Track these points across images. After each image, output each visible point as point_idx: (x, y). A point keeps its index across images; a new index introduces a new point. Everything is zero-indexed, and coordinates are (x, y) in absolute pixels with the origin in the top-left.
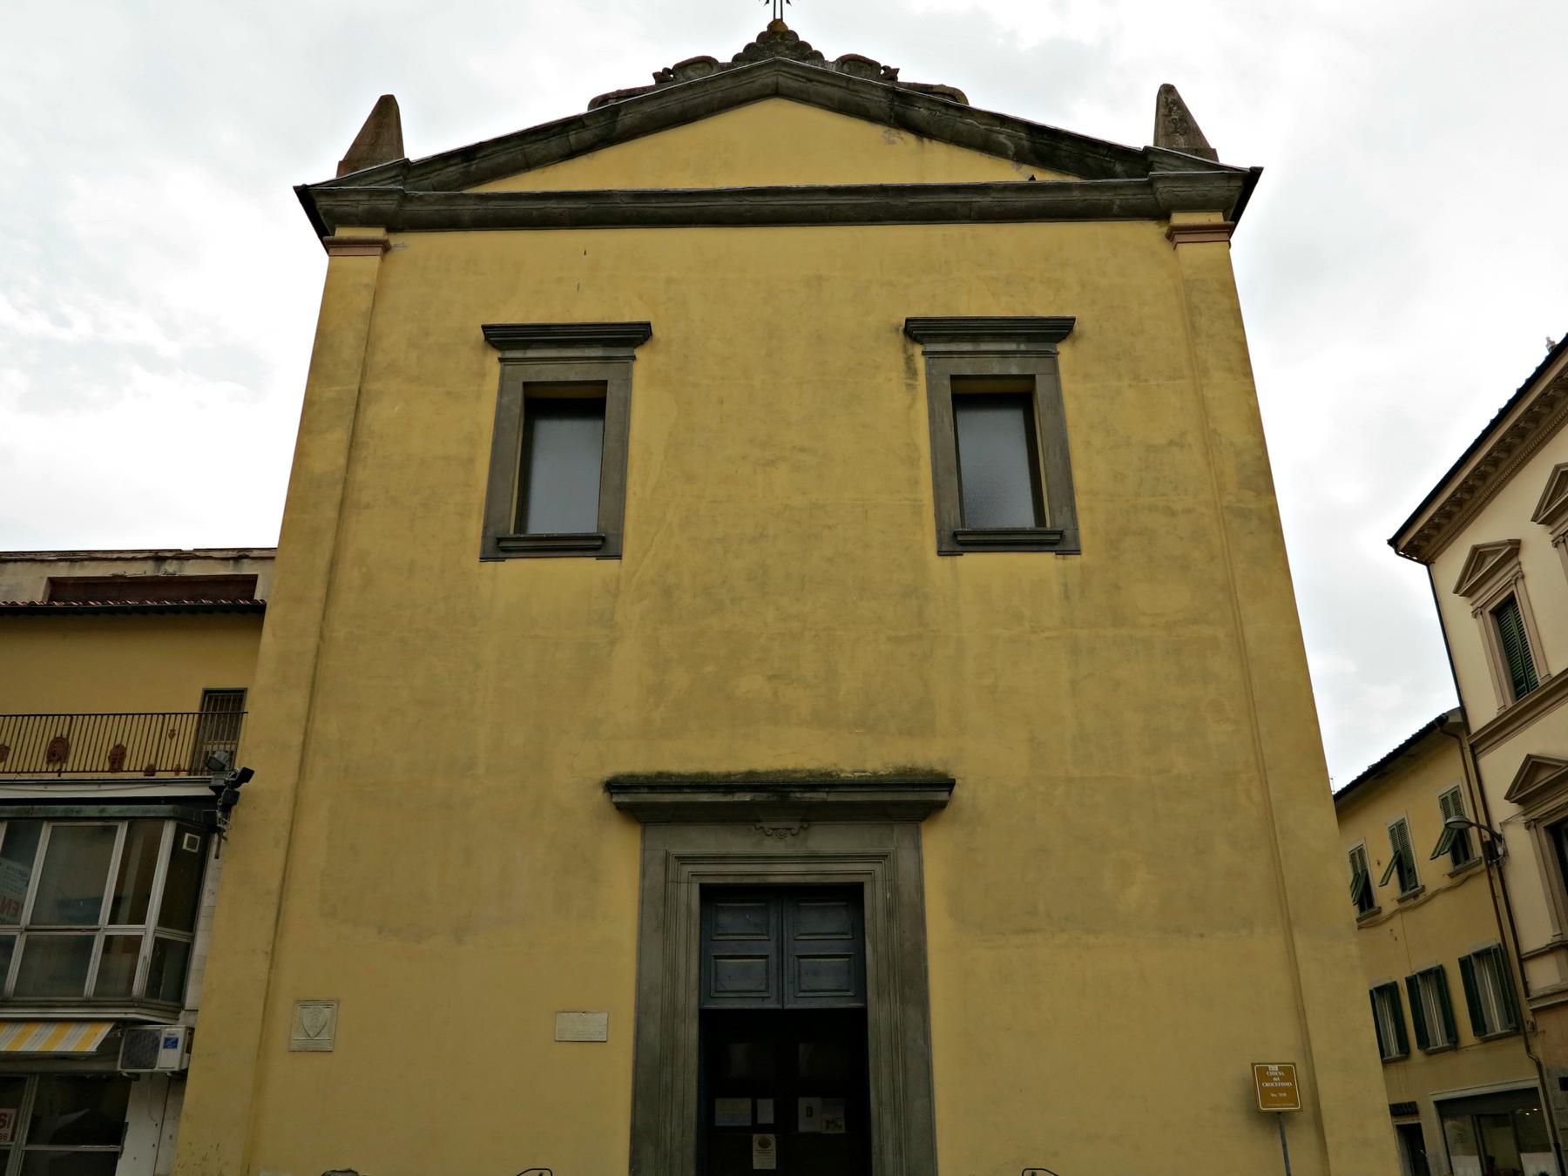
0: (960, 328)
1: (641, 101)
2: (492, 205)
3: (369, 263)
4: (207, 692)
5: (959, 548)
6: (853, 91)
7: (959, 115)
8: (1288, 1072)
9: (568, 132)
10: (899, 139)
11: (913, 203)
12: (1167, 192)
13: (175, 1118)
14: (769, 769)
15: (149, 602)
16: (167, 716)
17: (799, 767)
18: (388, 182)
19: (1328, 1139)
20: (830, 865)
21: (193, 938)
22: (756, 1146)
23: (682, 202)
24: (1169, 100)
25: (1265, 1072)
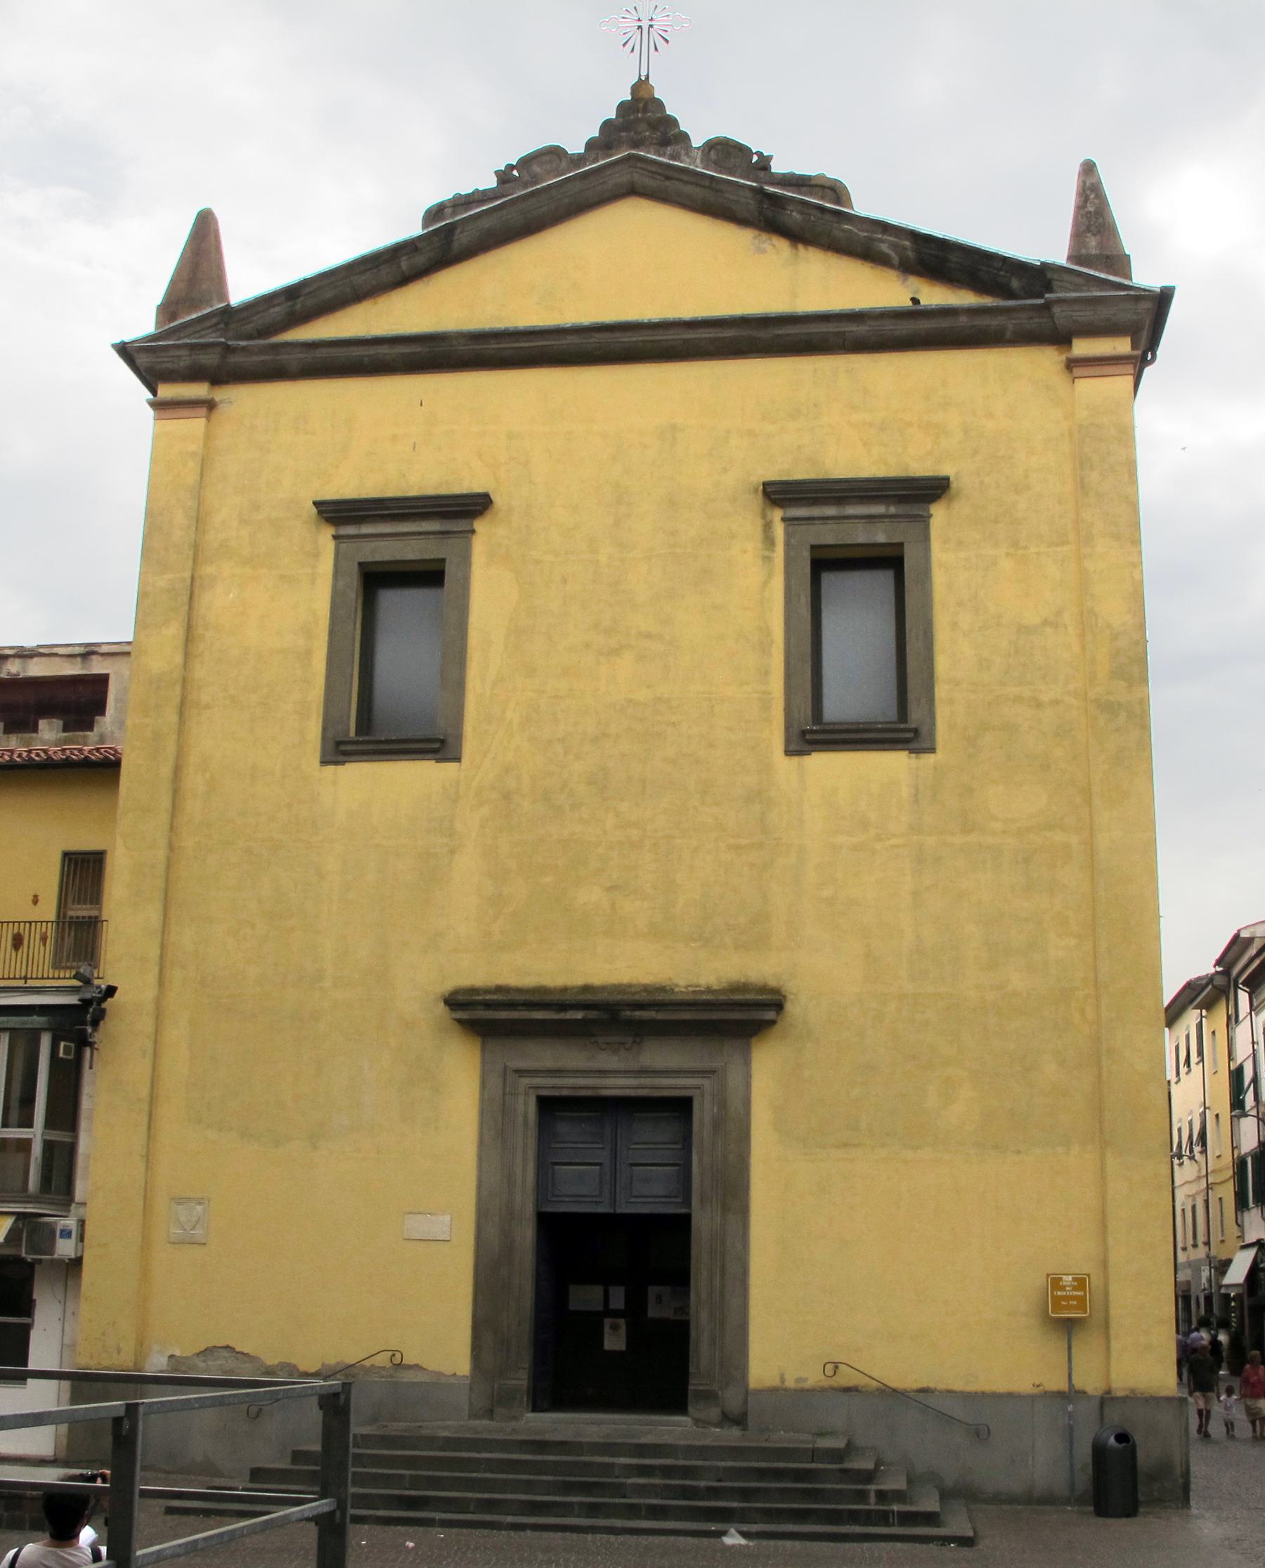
0: (823, 491)
2: (321, 353)
3: (192, 426)
4: (67, 855)
5: (807, 747)
8: (1081, 1283)
10: (771, 247)
11: (778, 336)
13: (75, 1297)
14: (605, 984)
16: (33, 924)
17: (634, 981)
21: (76, 1137)
22: (607, 1329)
25: (1059, 1281)
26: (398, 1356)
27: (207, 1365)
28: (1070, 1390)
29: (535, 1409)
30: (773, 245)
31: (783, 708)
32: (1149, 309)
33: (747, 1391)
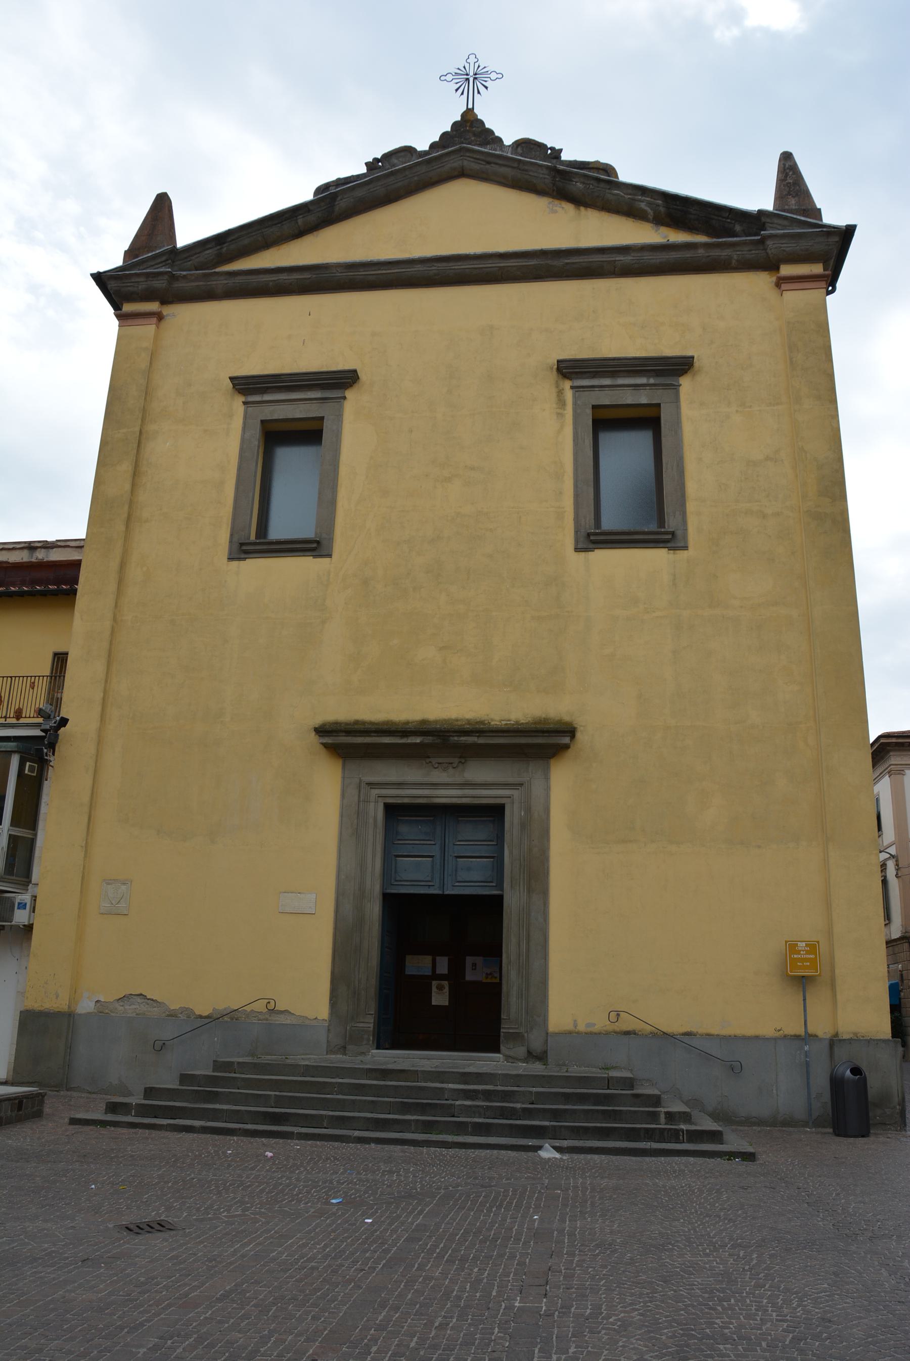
1: (353, 188)
2: (239, 279)
3: (147, 330)
5: (591, 546)
6: (523, 170)
7: (608, 187)
8: (813, 947)
9: (296, 217)
11: (567, 264)
12: (776, 248)
15: (12, 588)
17: (460, 717)
18: (161, 265)
19: (838, 997)
20: (482, 790)
21: (36, 835)
22: (434, 989)
23: (385, 270)
24: (787, 164)
26: (272, 1003)
27: (124, 1008)
28: (805, 1035)
29: (378, 1047)
30: (563, 208)
31: (573, 518)
32: (837, 242)
33: (547, 1034)
